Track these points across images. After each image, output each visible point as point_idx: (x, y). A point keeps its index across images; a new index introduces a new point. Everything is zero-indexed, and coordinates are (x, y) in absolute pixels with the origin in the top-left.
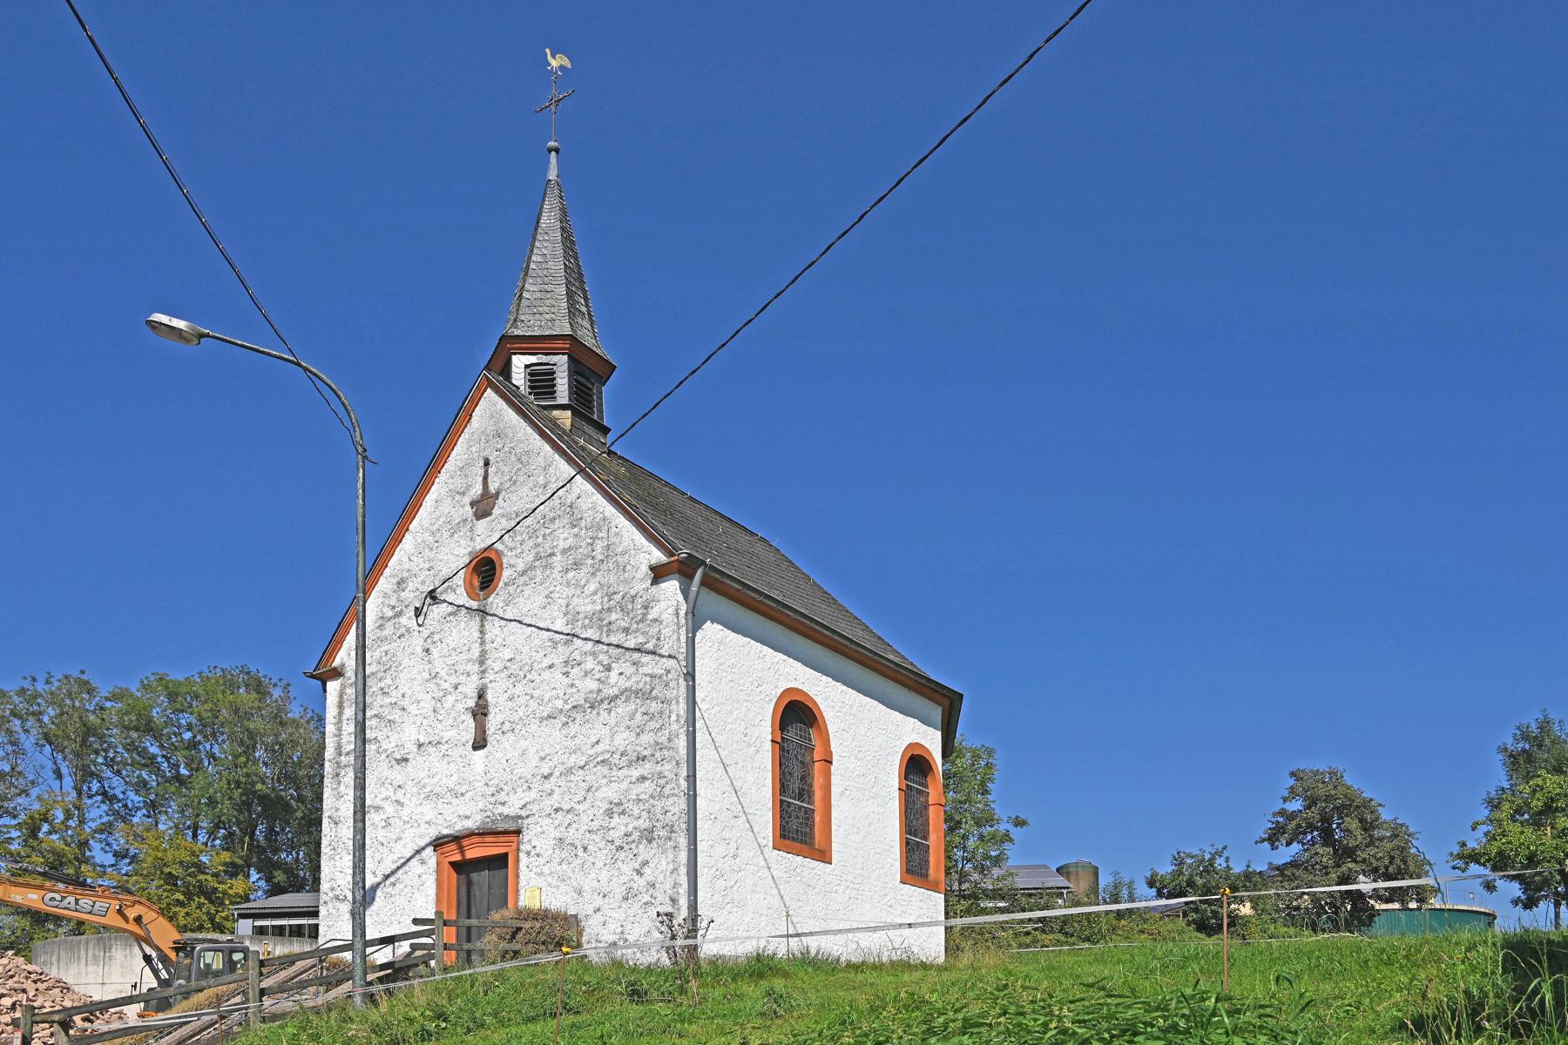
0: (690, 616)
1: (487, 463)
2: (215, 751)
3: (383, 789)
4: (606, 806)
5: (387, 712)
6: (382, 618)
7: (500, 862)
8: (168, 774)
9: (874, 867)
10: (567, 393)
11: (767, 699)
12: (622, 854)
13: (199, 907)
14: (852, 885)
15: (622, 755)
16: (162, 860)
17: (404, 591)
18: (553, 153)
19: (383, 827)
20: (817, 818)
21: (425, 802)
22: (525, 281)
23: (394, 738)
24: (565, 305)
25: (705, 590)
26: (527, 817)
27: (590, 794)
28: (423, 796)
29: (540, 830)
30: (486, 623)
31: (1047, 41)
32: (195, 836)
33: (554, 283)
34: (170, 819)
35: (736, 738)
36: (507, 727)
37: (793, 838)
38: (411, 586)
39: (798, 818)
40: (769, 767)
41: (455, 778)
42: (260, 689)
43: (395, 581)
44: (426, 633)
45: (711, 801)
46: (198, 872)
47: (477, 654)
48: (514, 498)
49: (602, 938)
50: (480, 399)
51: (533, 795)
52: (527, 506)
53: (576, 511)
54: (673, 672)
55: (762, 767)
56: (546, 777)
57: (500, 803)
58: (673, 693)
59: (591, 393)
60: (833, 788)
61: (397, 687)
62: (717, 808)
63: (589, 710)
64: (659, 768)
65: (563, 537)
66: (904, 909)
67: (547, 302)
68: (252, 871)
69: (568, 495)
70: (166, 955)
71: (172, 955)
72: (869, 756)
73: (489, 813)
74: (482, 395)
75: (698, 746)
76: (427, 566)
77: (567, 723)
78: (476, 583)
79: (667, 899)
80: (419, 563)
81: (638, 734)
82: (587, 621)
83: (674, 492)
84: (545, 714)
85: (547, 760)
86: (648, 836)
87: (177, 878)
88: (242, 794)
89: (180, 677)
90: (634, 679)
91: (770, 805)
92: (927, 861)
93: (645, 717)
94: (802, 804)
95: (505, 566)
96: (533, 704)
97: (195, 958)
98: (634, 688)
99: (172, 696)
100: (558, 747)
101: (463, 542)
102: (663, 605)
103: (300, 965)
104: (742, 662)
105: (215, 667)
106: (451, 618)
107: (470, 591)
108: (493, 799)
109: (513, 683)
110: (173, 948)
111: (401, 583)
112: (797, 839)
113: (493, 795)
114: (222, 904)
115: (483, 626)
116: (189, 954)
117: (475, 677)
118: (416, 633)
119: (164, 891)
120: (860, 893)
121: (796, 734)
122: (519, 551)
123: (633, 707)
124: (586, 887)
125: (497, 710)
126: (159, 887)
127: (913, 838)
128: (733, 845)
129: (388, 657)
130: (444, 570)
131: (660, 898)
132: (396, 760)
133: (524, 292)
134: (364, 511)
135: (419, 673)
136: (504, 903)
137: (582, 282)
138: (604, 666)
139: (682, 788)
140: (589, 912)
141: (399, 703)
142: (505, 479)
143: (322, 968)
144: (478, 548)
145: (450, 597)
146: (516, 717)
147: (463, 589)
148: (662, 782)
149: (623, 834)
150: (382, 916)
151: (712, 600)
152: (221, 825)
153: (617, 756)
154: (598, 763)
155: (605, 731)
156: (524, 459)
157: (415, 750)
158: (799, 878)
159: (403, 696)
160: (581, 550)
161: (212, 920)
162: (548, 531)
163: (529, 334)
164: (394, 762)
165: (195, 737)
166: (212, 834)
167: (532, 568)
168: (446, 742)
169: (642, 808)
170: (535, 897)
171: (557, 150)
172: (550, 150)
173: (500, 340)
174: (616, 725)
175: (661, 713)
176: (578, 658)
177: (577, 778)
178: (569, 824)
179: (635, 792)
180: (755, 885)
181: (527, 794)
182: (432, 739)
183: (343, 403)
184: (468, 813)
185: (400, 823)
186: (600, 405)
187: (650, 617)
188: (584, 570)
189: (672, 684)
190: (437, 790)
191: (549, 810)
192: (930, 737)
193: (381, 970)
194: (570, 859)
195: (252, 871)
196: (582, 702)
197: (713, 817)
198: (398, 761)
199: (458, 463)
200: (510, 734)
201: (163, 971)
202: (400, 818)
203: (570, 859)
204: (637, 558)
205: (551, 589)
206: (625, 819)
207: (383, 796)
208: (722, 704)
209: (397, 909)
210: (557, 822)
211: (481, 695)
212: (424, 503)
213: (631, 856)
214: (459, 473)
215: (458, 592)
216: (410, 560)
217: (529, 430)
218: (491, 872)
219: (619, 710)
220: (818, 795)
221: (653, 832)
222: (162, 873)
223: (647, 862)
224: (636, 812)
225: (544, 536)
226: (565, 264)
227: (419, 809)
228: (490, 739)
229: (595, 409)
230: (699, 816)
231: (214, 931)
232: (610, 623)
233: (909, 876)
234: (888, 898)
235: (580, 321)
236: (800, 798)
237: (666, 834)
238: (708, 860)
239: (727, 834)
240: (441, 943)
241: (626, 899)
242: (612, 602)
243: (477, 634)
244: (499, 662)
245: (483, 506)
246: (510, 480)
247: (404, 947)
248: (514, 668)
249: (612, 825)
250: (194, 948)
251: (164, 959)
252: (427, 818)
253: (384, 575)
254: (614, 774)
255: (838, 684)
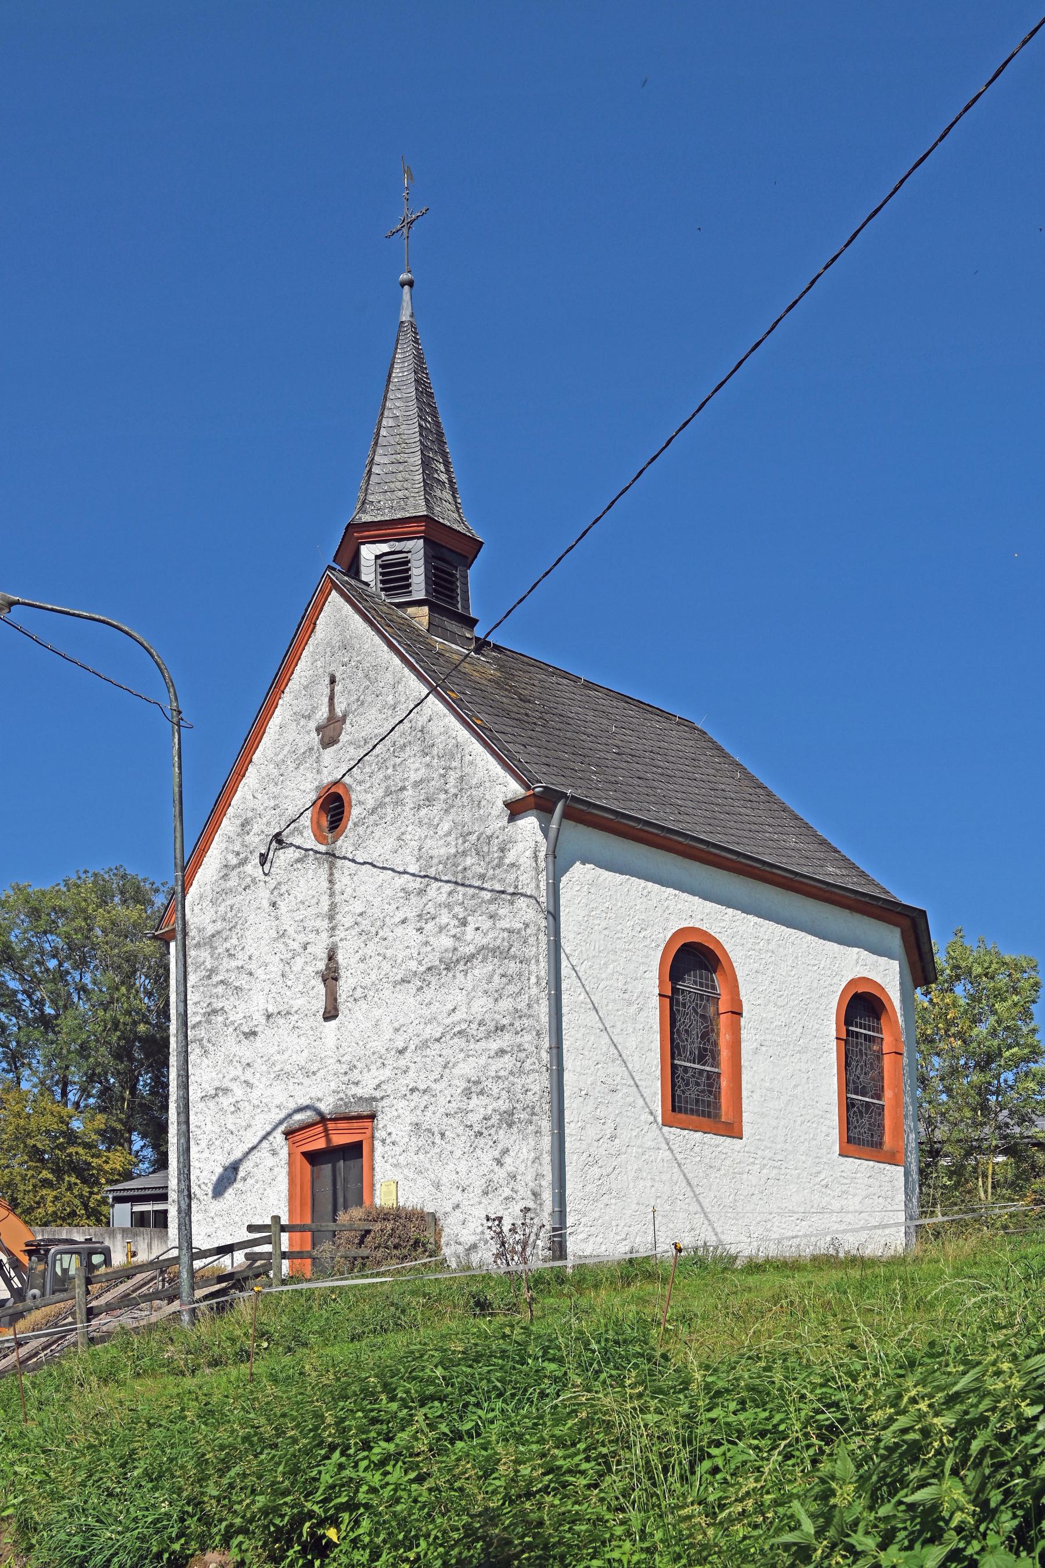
0: (550, 859)
1: (333, 681)
2: (87, 982)
3: (231, 1068)
4: (464, 1085)
5: (233, 977)
6: (226, 866)
7: (354, 1151)
8: (30, 1015)
9: (802, 1139)
10: (423, 585)
11: (653, 945)
12: (481, 1141)
13: (70, 1188)
14: (771, 1163)
15: (479, 1025)
16: (25, 1129)
17: (248, 834)
18: (406, 287)
19: (232, 1113)
20: (724, 1083)
21: (275, 1083)
22: (374, 452)
23: (242, 1007)
24: (419, 477)
25: (567, 823)
26: (382, 1098)
27: (447, 1071)
28: (272, 1076)
29: (396, 1114)
30: (335, 871)
31: (826, 268)
32: (64, 1094)
33: (407, 451)
34: (35, 1073)
35: (612, 997)
36: (359, 993)
37: (692, 1110)
38: (256, 828)
39: (698, 1084)
40: (657, 1027)
41: (305, 1054)
42: (137, 896)
43: (239, 822)
44: (272, 884)
45: (580, 1074)
46: (68, 1143)
47: (326, 908)
48: (362, 722)
49: (462, 1240)
50: (324, 604)
51: (387, 1073)
52: (376, 731)
53: (427, 736)
54: (532, 925)
55: (647, 1028)
56: (401, 1052)
57: (353, 1083)
58: (530, 952)
59: (454, 587)
60: (743, 1045)
61: (243, 948)
62: (589, 1083)
63: (444, 972)
64: (518, 1040)
65: (415, 768)
66: (845, 1188)
67: (400, 476)
68: (135, 1137)
69: (420, 718)
70: (18, 1260)
71: (24, 1259)
72: (794, 1000)
73: (342, 1095)
74: (326, 600)
75: (565, 1010)
76: (272, 804)
77: (422, 988)
78: (325, 823)
79: (529, 1192)
80: (264, 801)
81: (496, 1000)
82: (441, 867)
83: (565, 681)
84: (398, 978)
85: (401, 1032)
86: (508, 1119)
87: (44, 1152)
88: (119, 1038)
89: (35, 888)
90: (491, 935)
91: (658, 1073)
92: (881, 1126)
93: (504, 979)
94: (703, 1068)
95: (353, 803)
96: (386, 966)
97: (50, 1262)
98: (491, 946)
99: (35, 913)
100: (413, 1016)
101: (309, 775)
102: (520, 846)
103: (139, 1278)
104: (619, 904)
105: (86, 872)
106: (299, 865)
107: (318, 833)
108: (346, 1079)
109: (365, 941)
110: (25, 1251)
111: (245, 824)
112: (698, 1110)
113: (346, 1073)
114: (97, 1183)
115: (331, 874)
116: (43, 1258)
117: (324, 935)
118: (262, 883)
119: (28, 1169)
120: (783, 1171)
121: (695, 983)
122: (368, 785)
123: (491, 968)
124: (444, 1180)
125: (348, 974)
126: (21, 1164)
127: (860, 1098)
128: (610, 1125)
129: (234, 912)
130: (290, 808)
131: (522, 1191)
132: (244, 1034)
133: (374, 467)
134: (181, 780)
135: (266, 931)
136: (360, 1203)
137: (441, 443)
138: (459, 920)
139: (544, 1062)
140: (449, 1209)
141: (246, 966)
142: (352, 699)
143: (163, 1280)
144: (325, 782)
145: (297, 841)
146: (367, 982)
147: (310, 831)
148: (522, 1055)
149: (482, 1116)
150: (233, 1216)
151: (579, 835)
152: (96, 1079)
153: (474, 1026)
154: (455, 1035)
155: (461, 997)
156: (372, 674)
157: (264, 1021)
158: (698, 1159)
159: (250, 958)
160: (433, 783)
161: (85, 1205)
162: (398, 761)
163: (379, 518)
164: (241, 1036)
165: (60, 965)
166: (85, 1092)
167: (382, 805)
168: (296, 1012)
169: (501, 1087)
170: (391, 1192)
171: (410, 284)
172: (403, 285)
173: (347, 528)
174: (473, 989)
175: (520, 975)
176: (432, 911)
177: (433, 1053)
178: (426, 1107)
179: (494, 1068)
180: (640, 1170)
181: (381, 1071)
182: (281, 1008)
183: (156, 662)
184: (320, 1095)
185: (249, 1108)
186: (466, 592)
187: (507, 861)
188: (439, 806)
189: (532, 940)
190: (288, 1068)
191: (404, 1090)
192: (882, 968)
193: (219, 1282)
194: (428, 1148)
195: (135, 1137)
196: (437, 963)
197: (583, 1093)
198: (247, 1035)
199: (302, 681)
200: (362, 1002)
201: (16, 1279)
202: (249, 1101)
203: (428, 1148)
204: (492, 791)
205: (402, 830)
206: (484, 1100)
207: (231, 1076)
208: (594, 957)
209: (249, 1208)
210: (412, 1104)
211: (331, 957)
212: (267, 730)
213: (491, 1143)
214: (304, 692)
215: (305, 834)
216: (254, 797)
217: (377, 640)
218: (348, 1163)
219: (476, 972)
220: (724, 1054)
221: (513, 1114)
222: (26, 1146)
223: (508, 1150)
224: (495, 1091)
225: (394, 766)
226: (420, 425)
227: (269, 1091)
228: (341, 1008)
229: (459, 598)
230: (567, 1094)
231: (88, 1218)
232: (465, 869)
233: (852, 1147)
234: (822, 1176)
235: (438, 493)
236: (701, 1059)
237: (527, 1117)
238: (578, 1144)
239: (601, 1112)
240: (278, 1252)
241: (486, 1193)
242: (466, 844)
243: (325, 884)
244: (349, 917)
245: (329, 732)
246: (358, 700)
247: (239, 1256)
248: (365, 923)
249: (470, 1107)
250: (47, 1251)
251: (16, 1264)
252: (277, 1102)
253: (228, 816)
254: (472, 1047)
255: (750, 917)
